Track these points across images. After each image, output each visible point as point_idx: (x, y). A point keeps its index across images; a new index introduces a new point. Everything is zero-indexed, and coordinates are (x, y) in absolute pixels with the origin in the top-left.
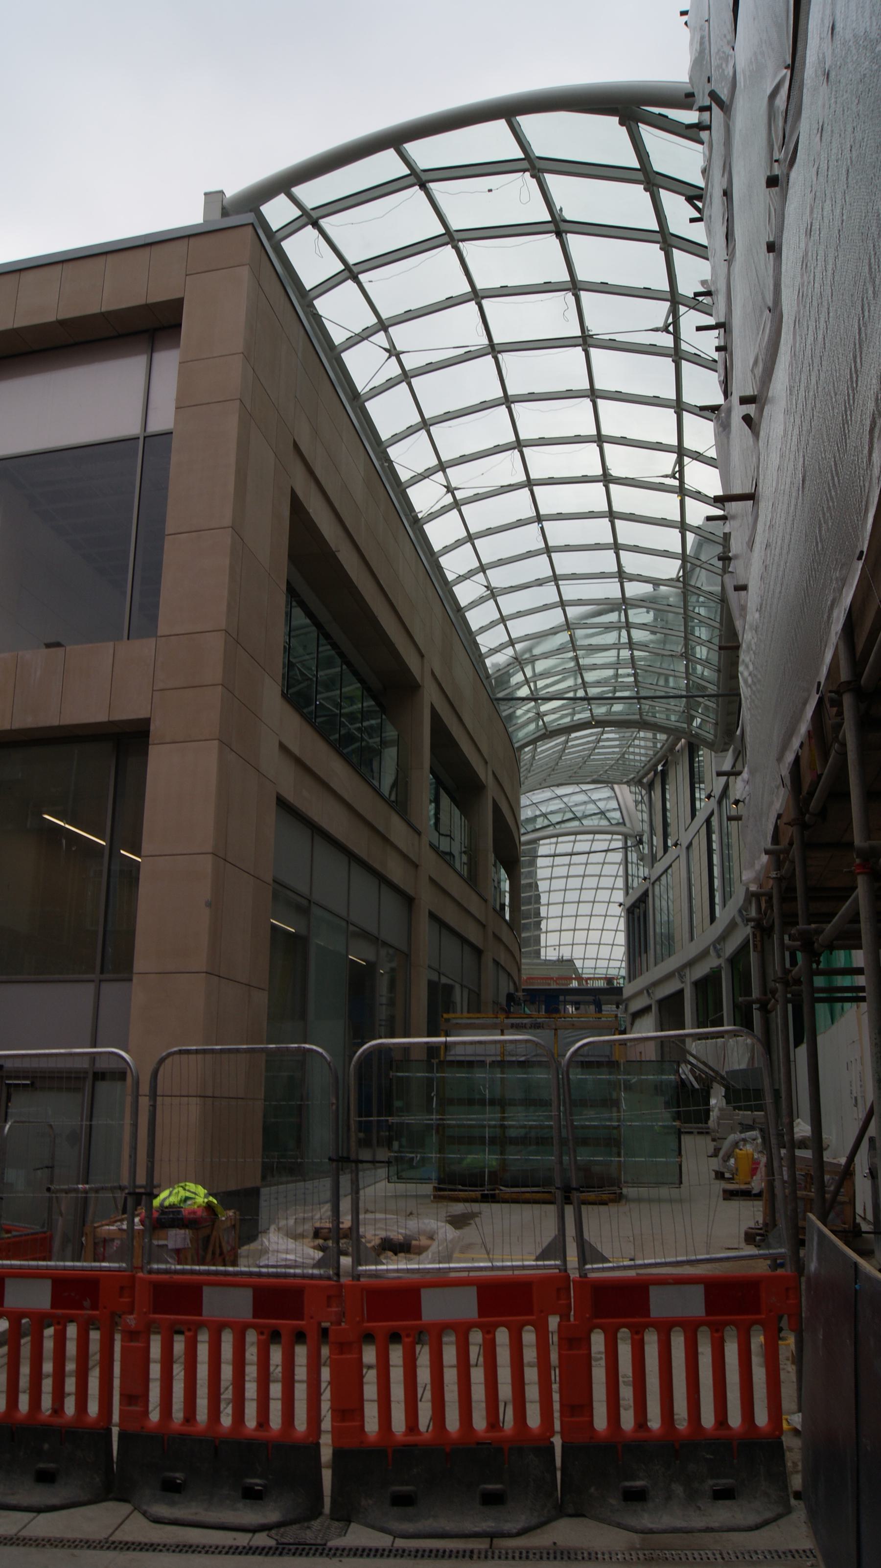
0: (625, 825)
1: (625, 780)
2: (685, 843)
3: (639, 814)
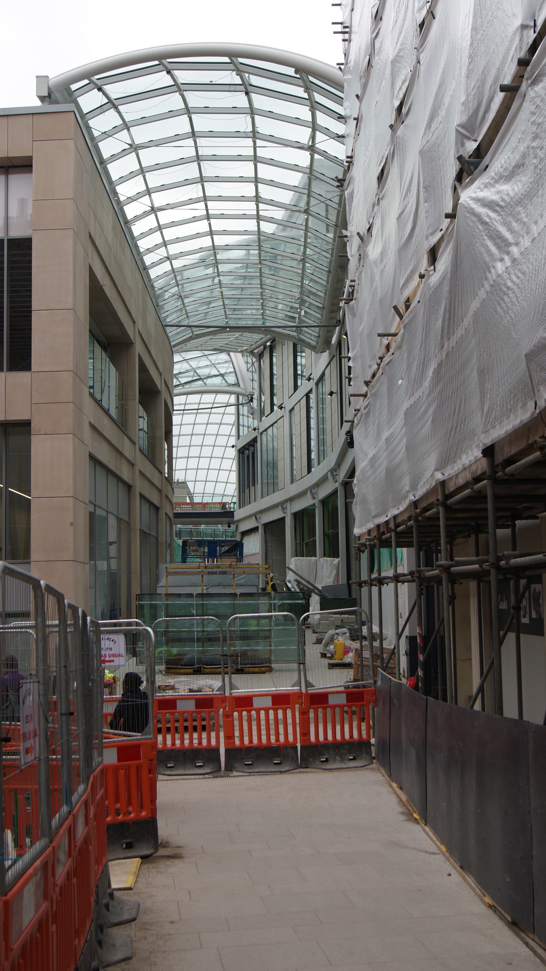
0: (239, 386)
1: (239, 350)
2: (288, 408)
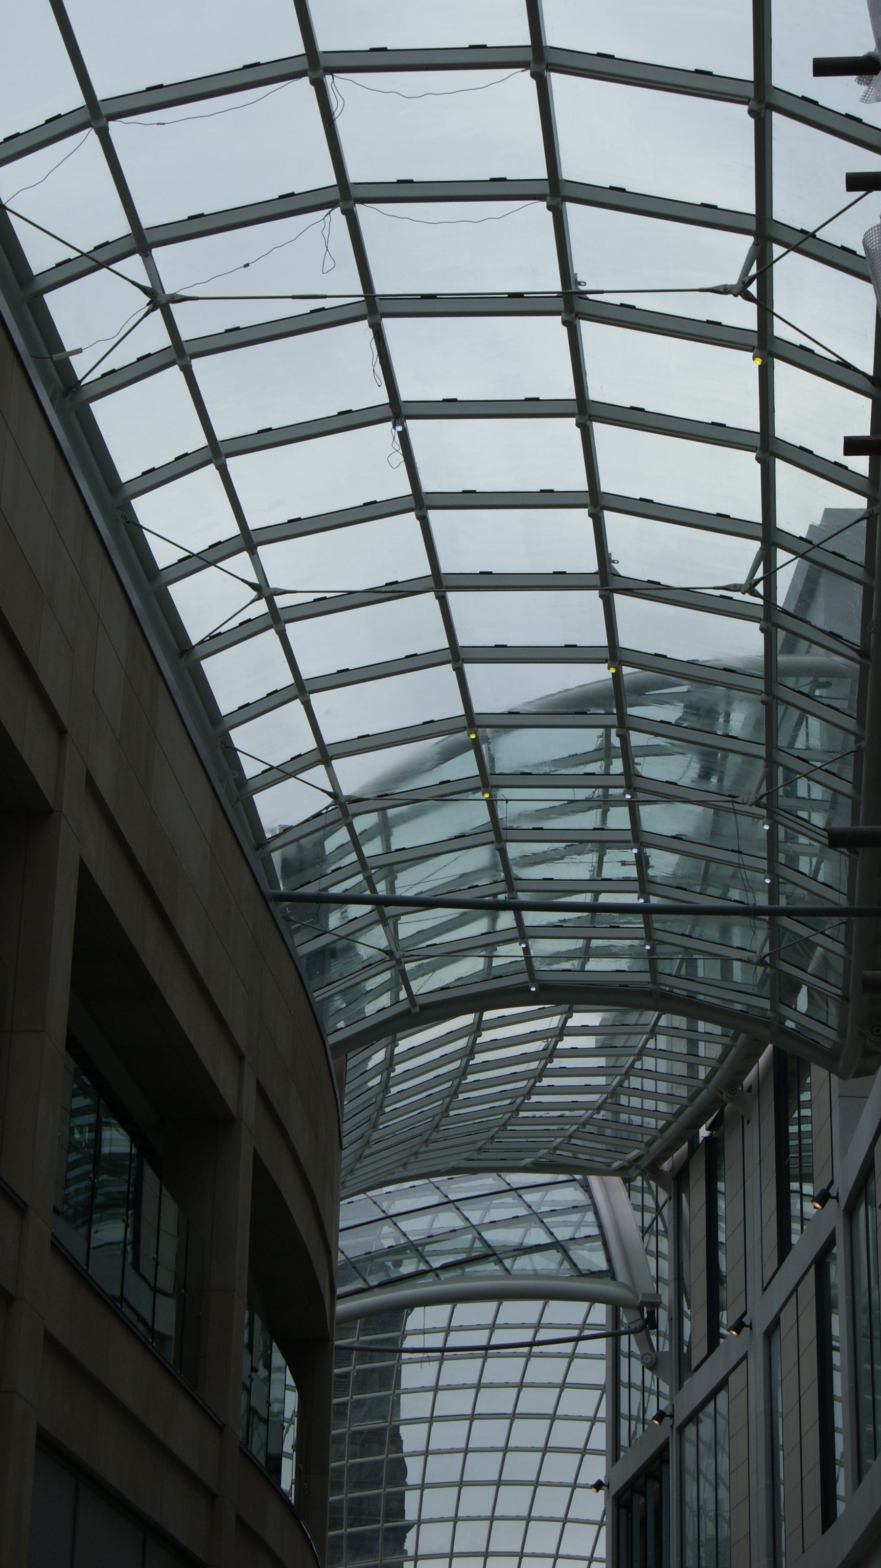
0: (614, 1277)
1: (616, 1164)
2: (761, 1324)
3: (652, 1261)
